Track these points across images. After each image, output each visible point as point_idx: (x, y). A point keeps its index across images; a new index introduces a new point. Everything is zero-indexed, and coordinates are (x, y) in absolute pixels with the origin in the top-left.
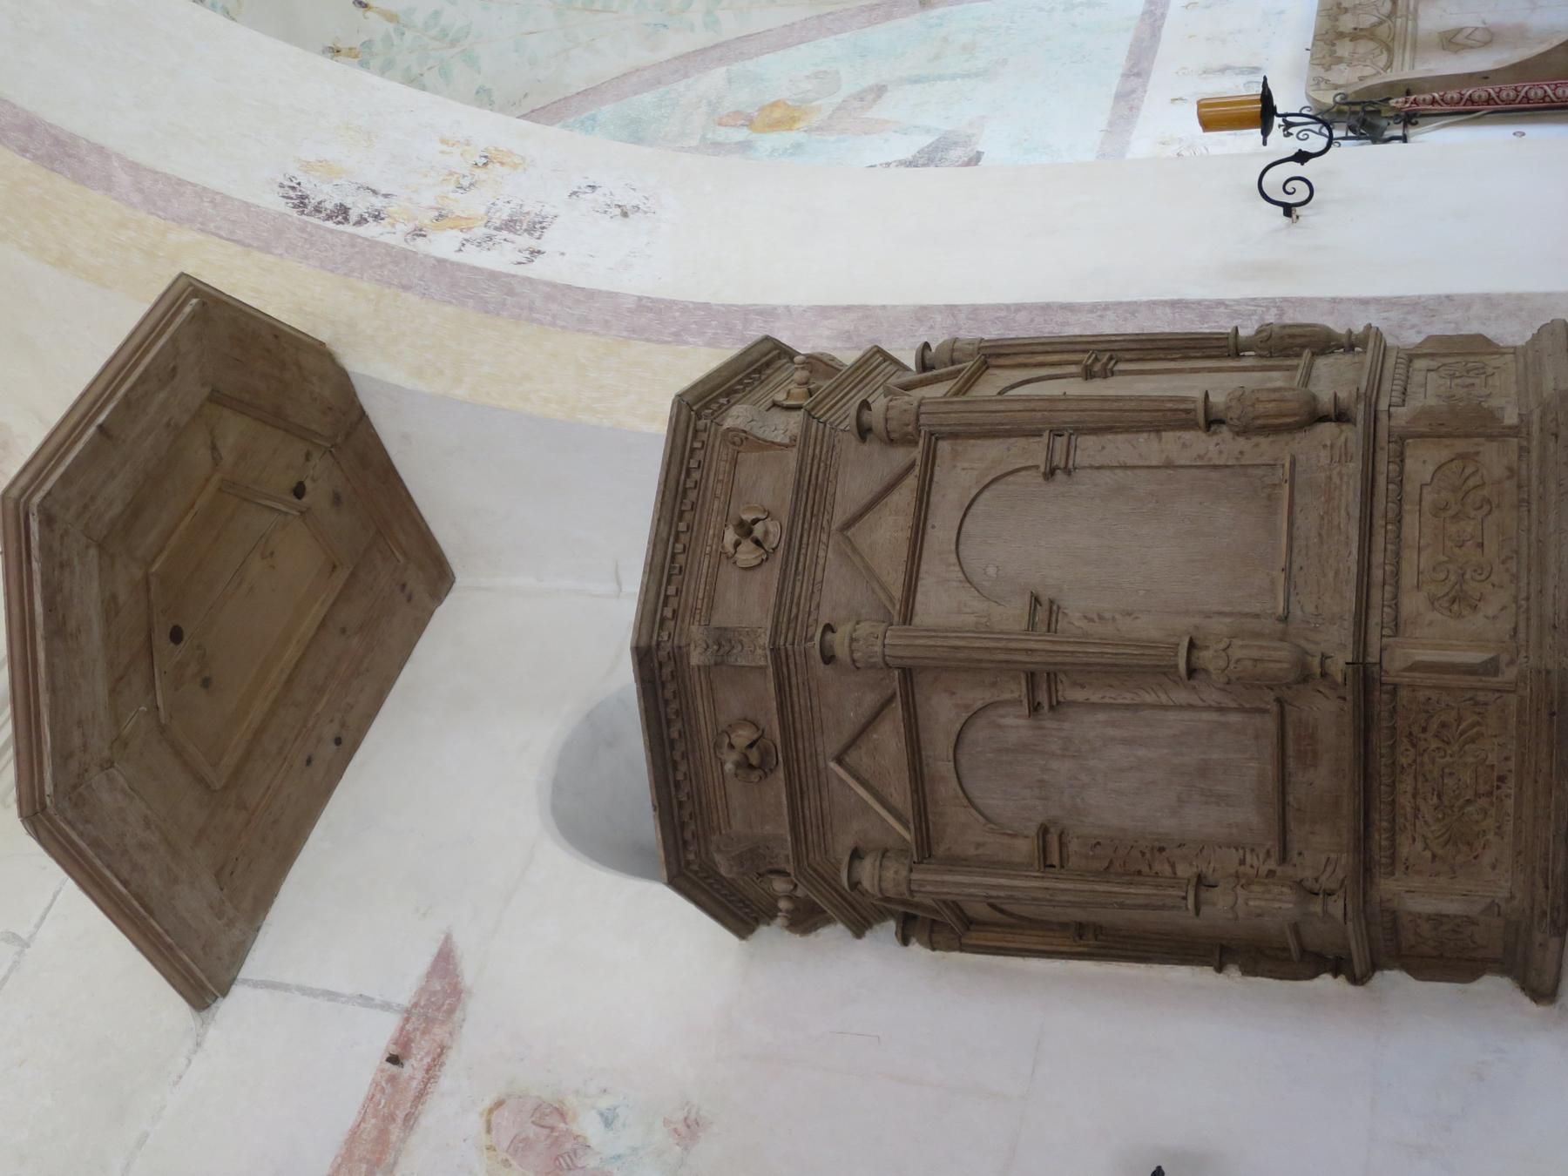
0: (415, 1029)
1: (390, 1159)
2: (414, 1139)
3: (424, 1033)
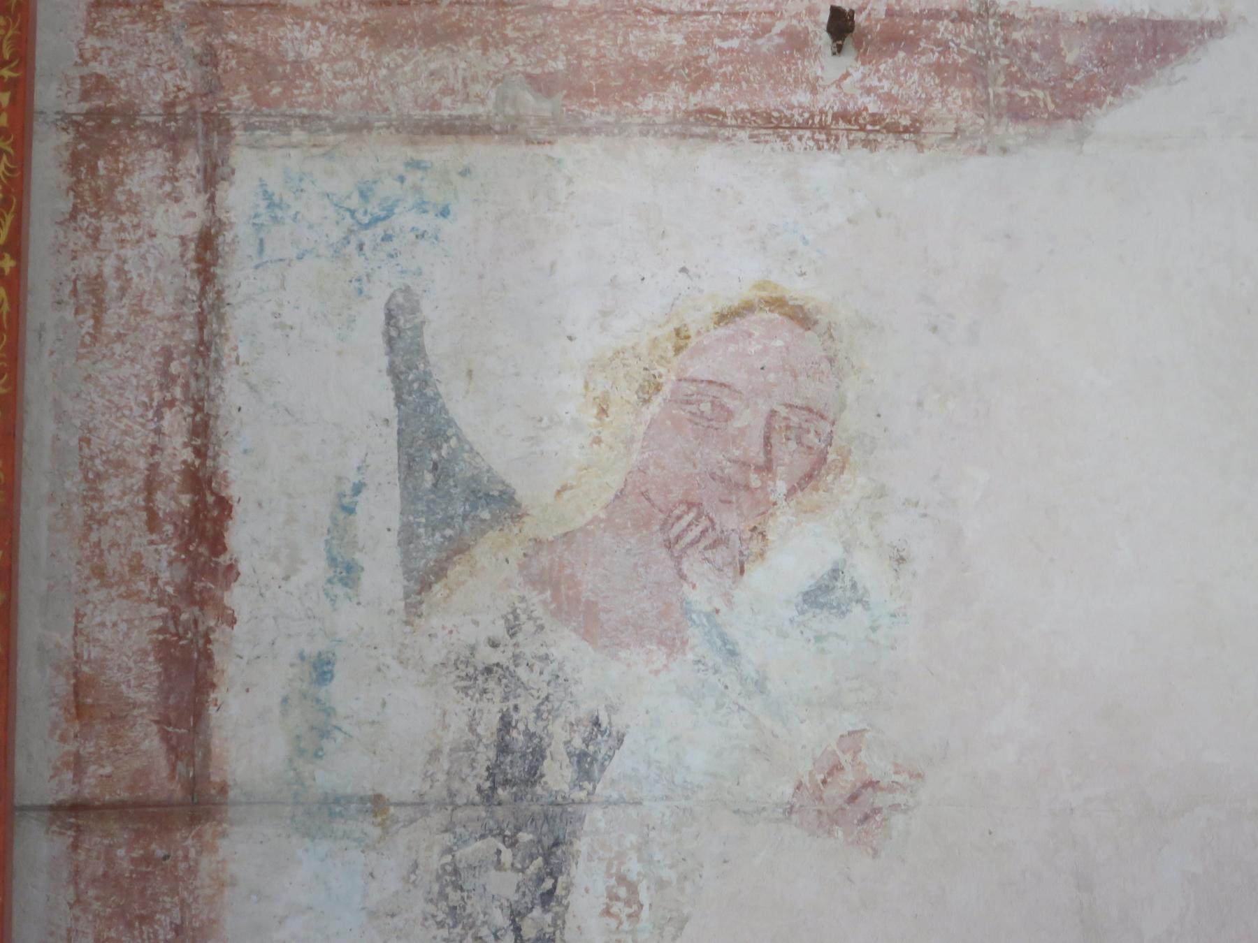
0: (944, 46)
1: (594, 116)
2: (657, 153)
3: (939, 69)
